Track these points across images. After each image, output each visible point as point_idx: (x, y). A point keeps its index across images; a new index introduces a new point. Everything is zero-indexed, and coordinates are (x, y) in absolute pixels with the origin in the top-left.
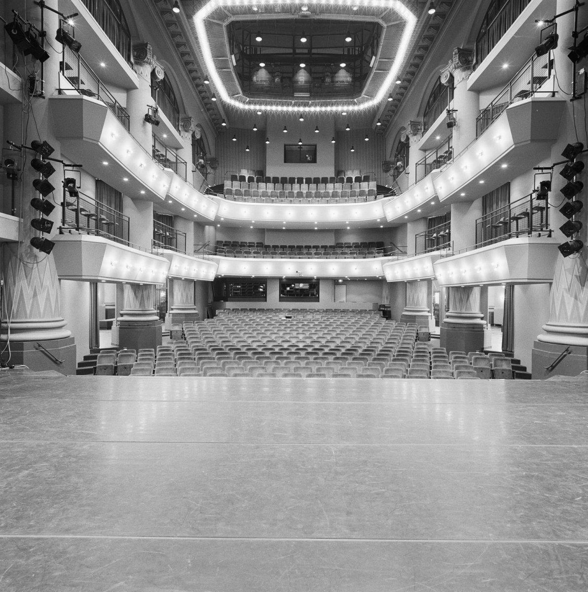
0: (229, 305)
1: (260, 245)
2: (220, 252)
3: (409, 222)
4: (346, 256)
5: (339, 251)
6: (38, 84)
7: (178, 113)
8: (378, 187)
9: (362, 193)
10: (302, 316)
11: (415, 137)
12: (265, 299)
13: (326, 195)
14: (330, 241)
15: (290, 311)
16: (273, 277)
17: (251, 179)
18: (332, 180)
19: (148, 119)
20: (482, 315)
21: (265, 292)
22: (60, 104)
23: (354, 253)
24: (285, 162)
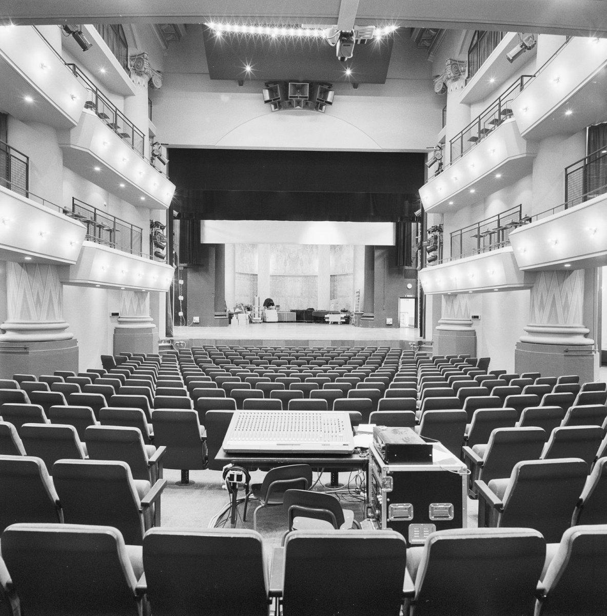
7: (126, 46)
10: (417, 527)
11: (456, 84)
16: (113, 343)
20: (587, 331)
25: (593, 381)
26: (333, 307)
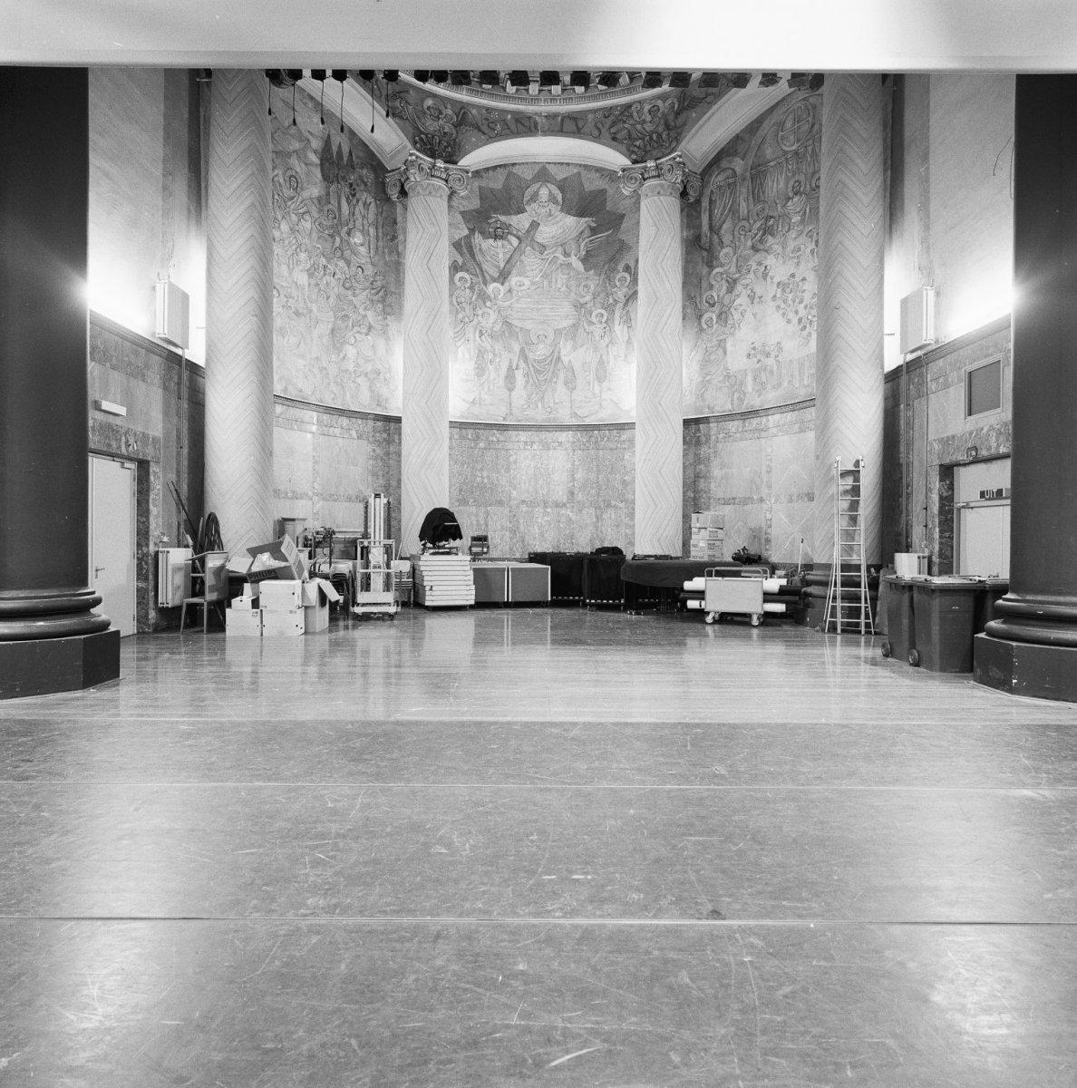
25: (210, 592)
26: (702, 544)
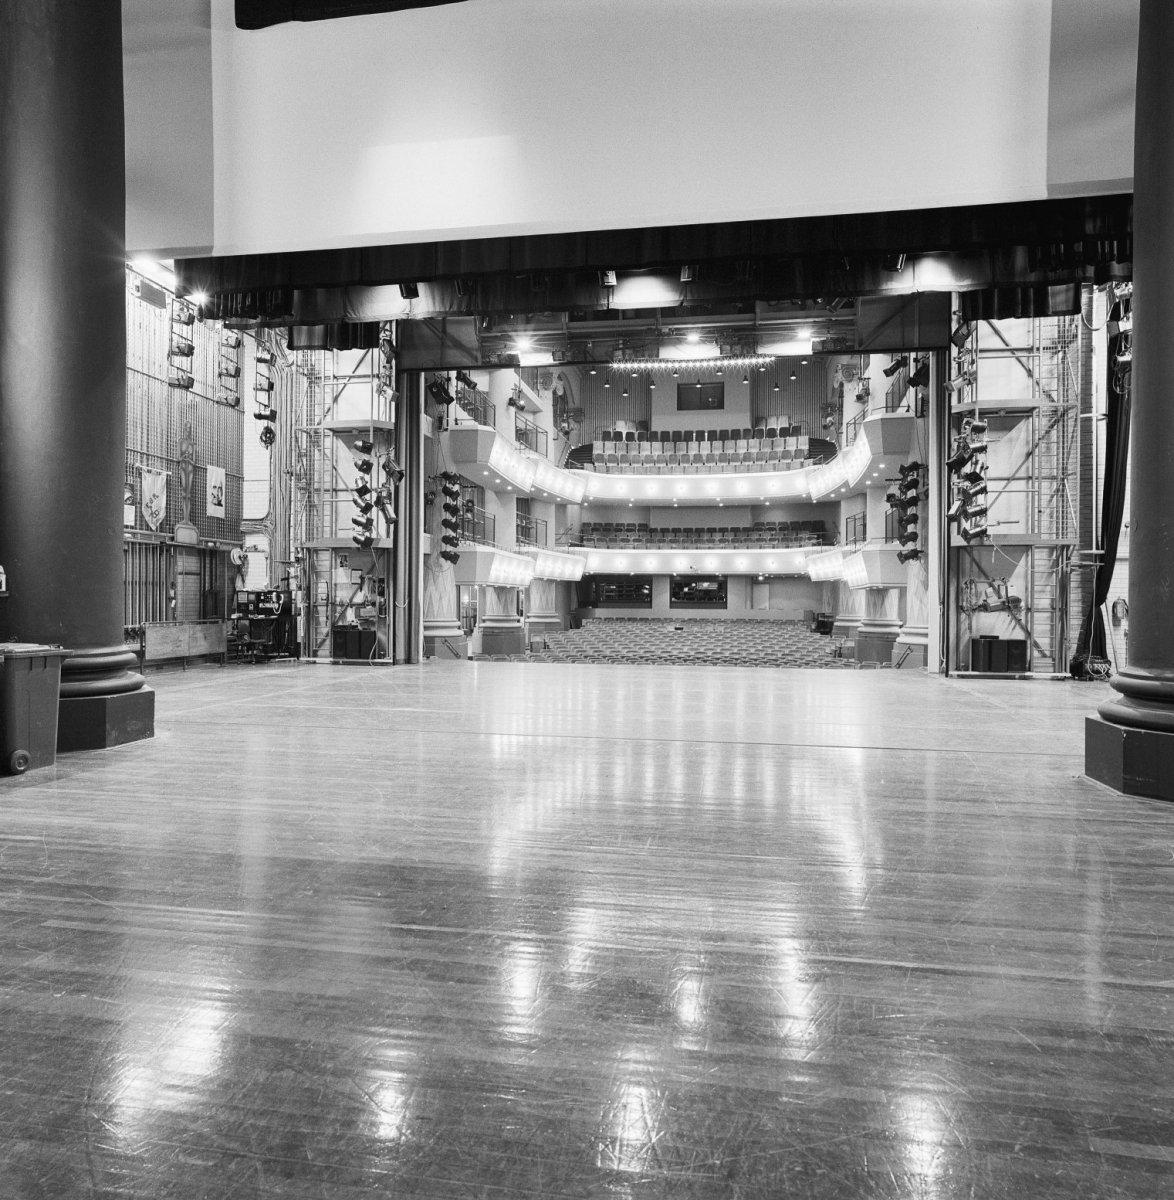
0: (600, 612)
1: (644, 528)
2: (589, 540)
3: (843, 499)
4: (763, 543)
5: (755, 536)
6: (445, 422)
8: (812, 442)
9: (786, 455)
12: (649, 605)
13: (735, 458)
14: (745, 522)
15: (684, 621)
17: (630, 436)
18: (747, 434)
19: (512, 402)
21: (650, 595)
22: (458, 435)
23: (774, 540)
24: (680, 408)
